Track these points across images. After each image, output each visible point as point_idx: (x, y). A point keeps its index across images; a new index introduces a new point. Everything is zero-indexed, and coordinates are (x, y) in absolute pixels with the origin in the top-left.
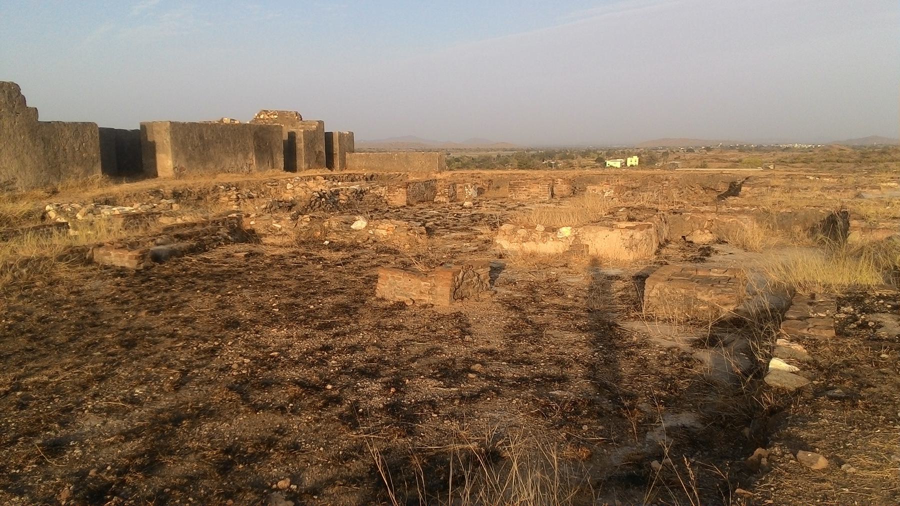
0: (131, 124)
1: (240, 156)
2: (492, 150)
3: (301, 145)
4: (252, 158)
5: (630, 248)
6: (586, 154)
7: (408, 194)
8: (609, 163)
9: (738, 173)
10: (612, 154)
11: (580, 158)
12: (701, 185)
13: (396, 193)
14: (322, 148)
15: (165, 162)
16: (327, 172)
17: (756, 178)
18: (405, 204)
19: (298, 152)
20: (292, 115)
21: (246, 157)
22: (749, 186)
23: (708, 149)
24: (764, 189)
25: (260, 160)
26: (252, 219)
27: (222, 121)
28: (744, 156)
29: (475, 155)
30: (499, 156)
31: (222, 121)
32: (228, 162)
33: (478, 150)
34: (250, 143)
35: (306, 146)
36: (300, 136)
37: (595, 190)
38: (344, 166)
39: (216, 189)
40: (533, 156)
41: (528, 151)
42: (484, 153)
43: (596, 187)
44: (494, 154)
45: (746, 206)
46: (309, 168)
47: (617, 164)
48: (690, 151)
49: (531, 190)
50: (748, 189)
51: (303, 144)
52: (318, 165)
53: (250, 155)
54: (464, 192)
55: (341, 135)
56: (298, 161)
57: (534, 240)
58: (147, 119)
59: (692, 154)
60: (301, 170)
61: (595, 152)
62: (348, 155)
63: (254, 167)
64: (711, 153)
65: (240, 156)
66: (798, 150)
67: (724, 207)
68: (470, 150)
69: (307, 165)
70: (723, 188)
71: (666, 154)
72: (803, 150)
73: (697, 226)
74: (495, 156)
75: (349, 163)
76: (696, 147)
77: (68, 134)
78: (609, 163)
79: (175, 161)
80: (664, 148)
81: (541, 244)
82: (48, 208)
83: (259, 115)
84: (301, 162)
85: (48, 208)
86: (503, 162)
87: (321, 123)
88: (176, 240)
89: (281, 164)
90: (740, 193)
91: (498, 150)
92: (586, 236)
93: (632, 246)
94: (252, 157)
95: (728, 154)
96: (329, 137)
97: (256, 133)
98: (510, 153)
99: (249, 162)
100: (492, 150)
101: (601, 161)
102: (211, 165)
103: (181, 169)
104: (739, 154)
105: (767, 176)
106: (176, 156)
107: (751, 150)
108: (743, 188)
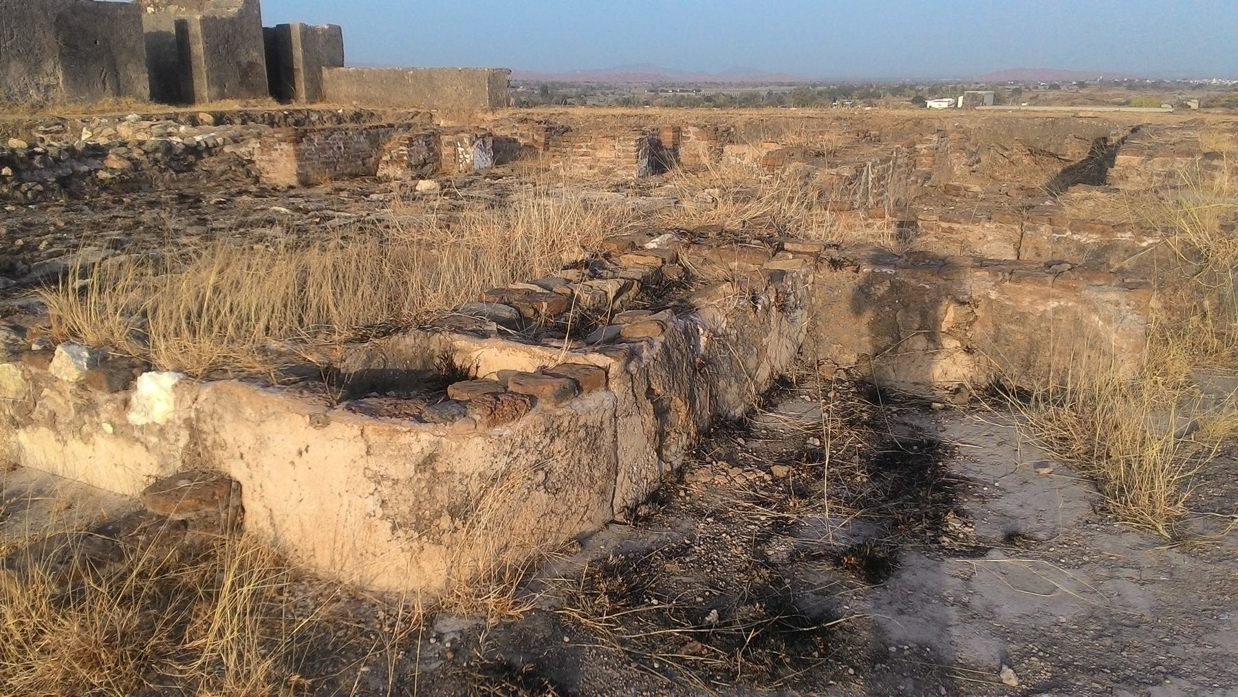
2: (762, 84)
4: (55, 74)
5: (420, 525)
6: (898, 91)
7: (300, 156)
8: (930, 103)
9: (1115, 117)
10: (937, 91)
11: (889, 96)
12: (1025, 142)
13: (275, 155)
16: (271, 106)
17: (1157, 130)
18: (294, 181)
19: (194, 63)
21: (35, 68)
22: (1139, 151)
23: (1082, 85)
24: (1180, 165)
28: (1133, 95)
29: (736, 92)
30: (770, 94)
33: (742, 85)
34: (48, 39)
35: (212, 51)
36: (196, 29)
37: (741, 156)
38: (316, 93)
40: (820, 93)
41: (814, 86)
42: (750, 89)
43: (745, 149)
44: (763, 91)
45: (1121, 227)
46: (222, 96)
47: (944, 104)
48: (1054, 87)
49: (600, 154)
50: (1135, 160)
52: (245, 86)
53: (48, 66)
54: (456, 154)
55: (308, 33)
56: (196, 81)
57: (52, 421)
59: (1057, 92)
60: (202, 100)
61: (912, 87)
62: (326, 73)
64: (1084, 91)
66: (1216, 87)
67: (1045, 229)
68: (731, 85)
69: (215, 90)
70: (1076, 152)
71: (1018, 92)
72: (1223, 87)
73: (916, 321)
74: (765, 94)
75: (328, 89)
76: (1064, 83)
78: (930, 103)
80: (1016, 82)
81: (75, 445)
84: (202, 84)
86: (778, 101)
90: (1113, 173)
91: (771, 84)
92: (227, 435)
93: (434, 513)
95: (1110, 93)
97: (60, 17)
98: (787, 89)
99: (44, 81)
100: (762, 84)
101: (920, 101)
104: (1127, 92)
105: (1185, 126)
107: (1144, 87)
108: (1121, 159)
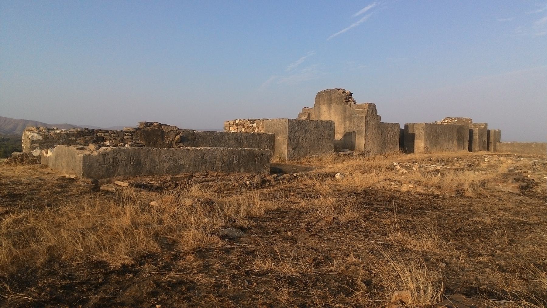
0: (434, 122)
1: (451, 142)
3: (476, 137)
14: (485, 139)
15: (420, 144)
20: (467, 120)
25: (459, 145)
26: (529, 174)
27: (436, 122)
31: (436, 122)
32: (446, 145)
34: (455, 135)
39: (453, 159)
51: (477, 136)
52: (484, 150)
55: (495, 131)
58: (410, 121)
60: (475, 151)
63: (456, 148)
65: (451, 142)
75: (498, 148)
77: (389, 128)
79: (425, 144)
82: (395, 164)
83: (444, 120)
84: (476, 147)
85: (395, 164)
87: (486, 124)
88: (536, 181)
89: (467, 148)
94: (455, 142)
96: (489, 131)
97: (458, 129)
102: (439, 147)
103: (428, 148)
106: (426, 141)
